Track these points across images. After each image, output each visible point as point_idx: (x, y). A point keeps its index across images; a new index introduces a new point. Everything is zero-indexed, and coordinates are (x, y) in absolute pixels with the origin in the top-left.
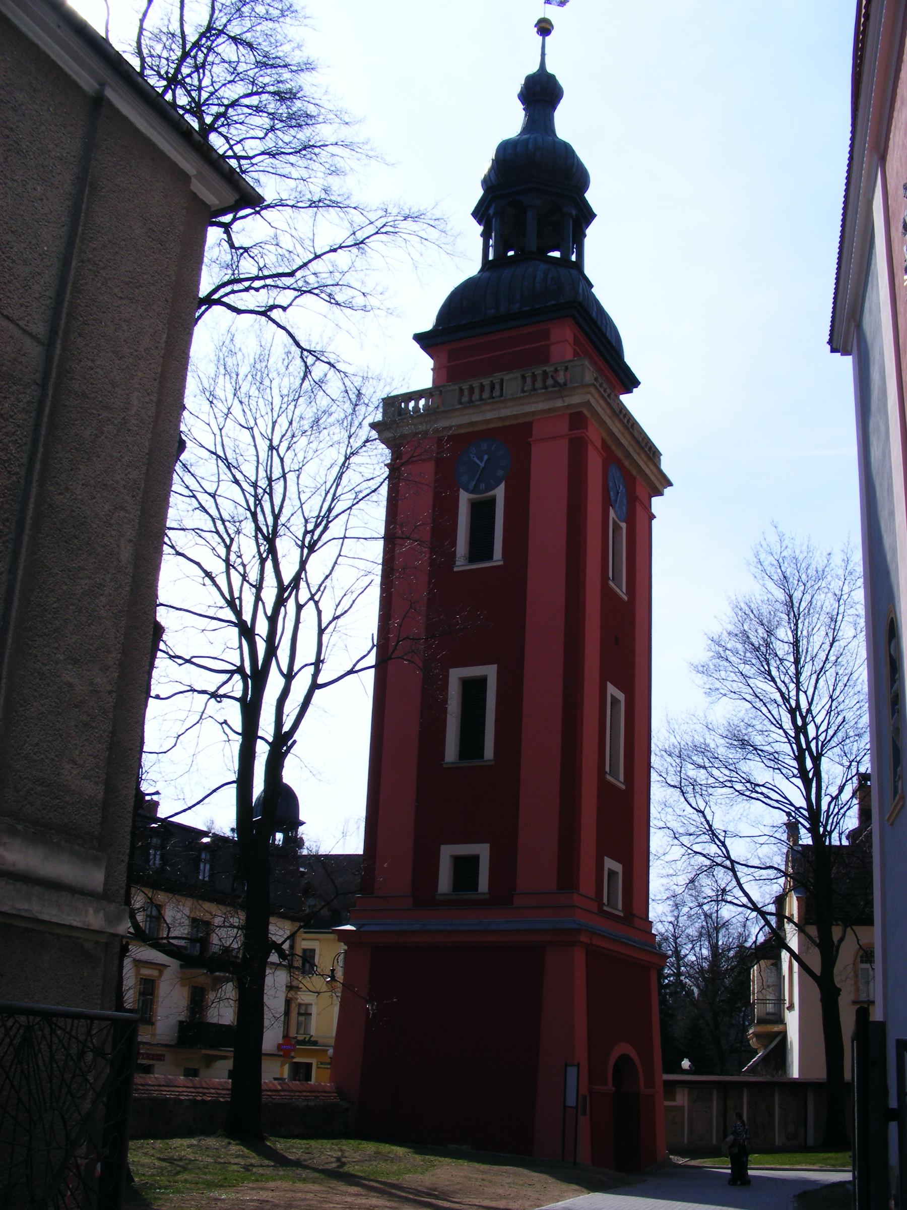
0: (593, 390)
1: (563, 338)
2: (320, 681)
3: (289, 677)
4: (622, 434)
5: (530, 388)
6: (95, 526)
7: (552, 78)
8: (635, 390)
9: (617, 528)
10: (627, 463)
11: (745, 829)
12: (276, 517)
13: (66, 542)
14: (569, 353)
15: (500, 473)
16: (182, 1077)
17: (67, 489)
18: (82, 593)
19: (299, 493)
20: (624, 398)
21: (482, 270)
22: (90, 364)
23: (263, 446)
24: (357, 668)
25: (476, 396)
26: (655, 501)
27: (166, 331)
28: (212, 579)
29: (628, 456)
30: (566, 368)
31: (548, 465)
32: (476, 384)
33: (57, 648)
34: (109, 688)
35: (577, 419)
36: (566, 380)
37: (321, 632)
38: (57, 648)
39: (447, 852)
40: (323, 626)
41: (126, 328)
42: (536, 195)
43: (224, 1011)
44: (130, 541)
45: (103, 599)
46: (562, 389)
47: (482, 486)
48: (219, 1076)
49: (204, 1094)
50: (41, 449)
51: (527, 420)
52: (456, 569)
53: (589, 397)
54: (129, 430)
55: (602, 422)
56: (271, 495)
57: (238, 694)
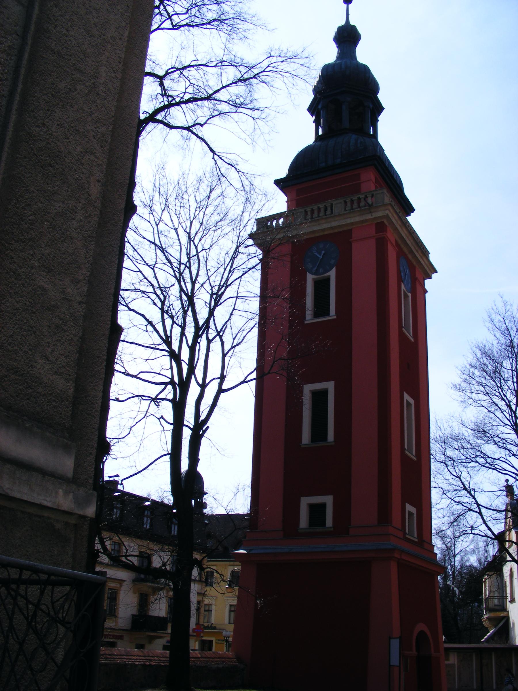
0: (390, 208)
1: (369, 178)
2: (224, 387)
3: (203, 386)
4: (408, 237)
5: (350, 208)
6: (68, 161)
7: (354, 28)
8: (411, 214)
9: (406, 296)
10: (410, 257)
11: (487, 487)
12: (193, 283)
13: (42, 167)
14: (372, 186)
15: (333, 262)
16: (136, 650)
17: (44, 124)
18: (56, 213)
19: (207, 271)
20: (407, 218)
21: (316, 141)
22: (65, 32)
23: (184, 239)
24: (247, 379)
25: (315, 215)
26: (426, 281)
27: (128, 29)
28: (153, 326)
29: (411, 252)
30: (373, 195)
31: (363, 255)
32: (315, 208)
33: (32, 255)
34: (79, 299)
35: (380, 226)
36: (372, 203)
37: (224, 355)
38: (32, 255)
39: (305, 502)
40: (225, 352)
41: (94, 14)
42: (347, 96)
43: (160, 608)
44: (99, 181)
45: (74, 222)
46: (370, 207)
47: (321, 270)
48: (158, 649)
49: (151, 660)
50: (20, 86)
51: (349, 228)
52: (306, 322)
53: (387, 212)
54: (98, 94)
55: (396, 229)
56: (190, 268)
57: (171, 397)
